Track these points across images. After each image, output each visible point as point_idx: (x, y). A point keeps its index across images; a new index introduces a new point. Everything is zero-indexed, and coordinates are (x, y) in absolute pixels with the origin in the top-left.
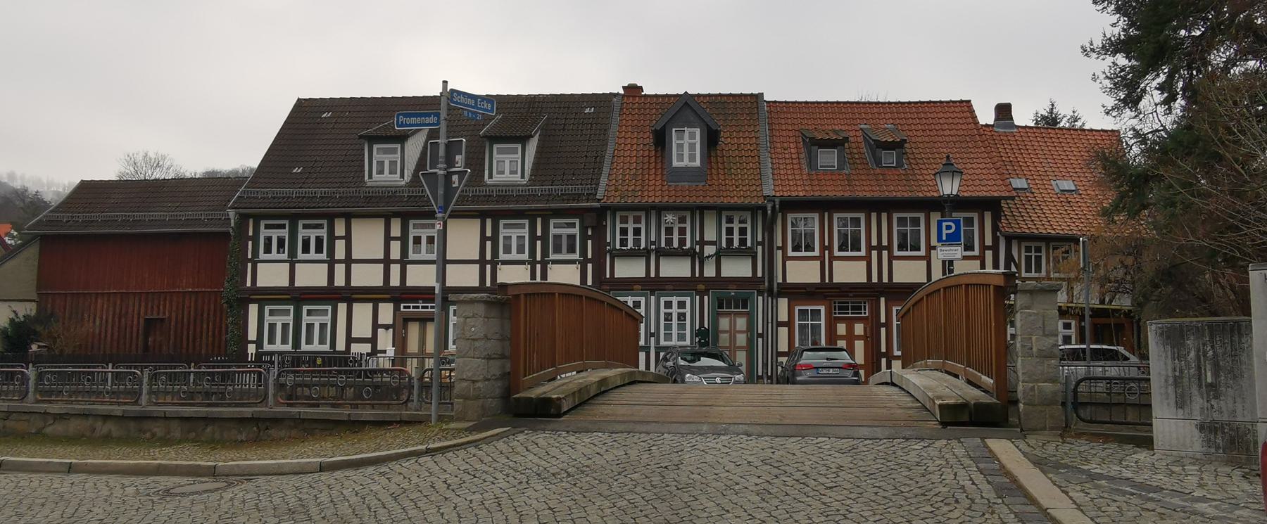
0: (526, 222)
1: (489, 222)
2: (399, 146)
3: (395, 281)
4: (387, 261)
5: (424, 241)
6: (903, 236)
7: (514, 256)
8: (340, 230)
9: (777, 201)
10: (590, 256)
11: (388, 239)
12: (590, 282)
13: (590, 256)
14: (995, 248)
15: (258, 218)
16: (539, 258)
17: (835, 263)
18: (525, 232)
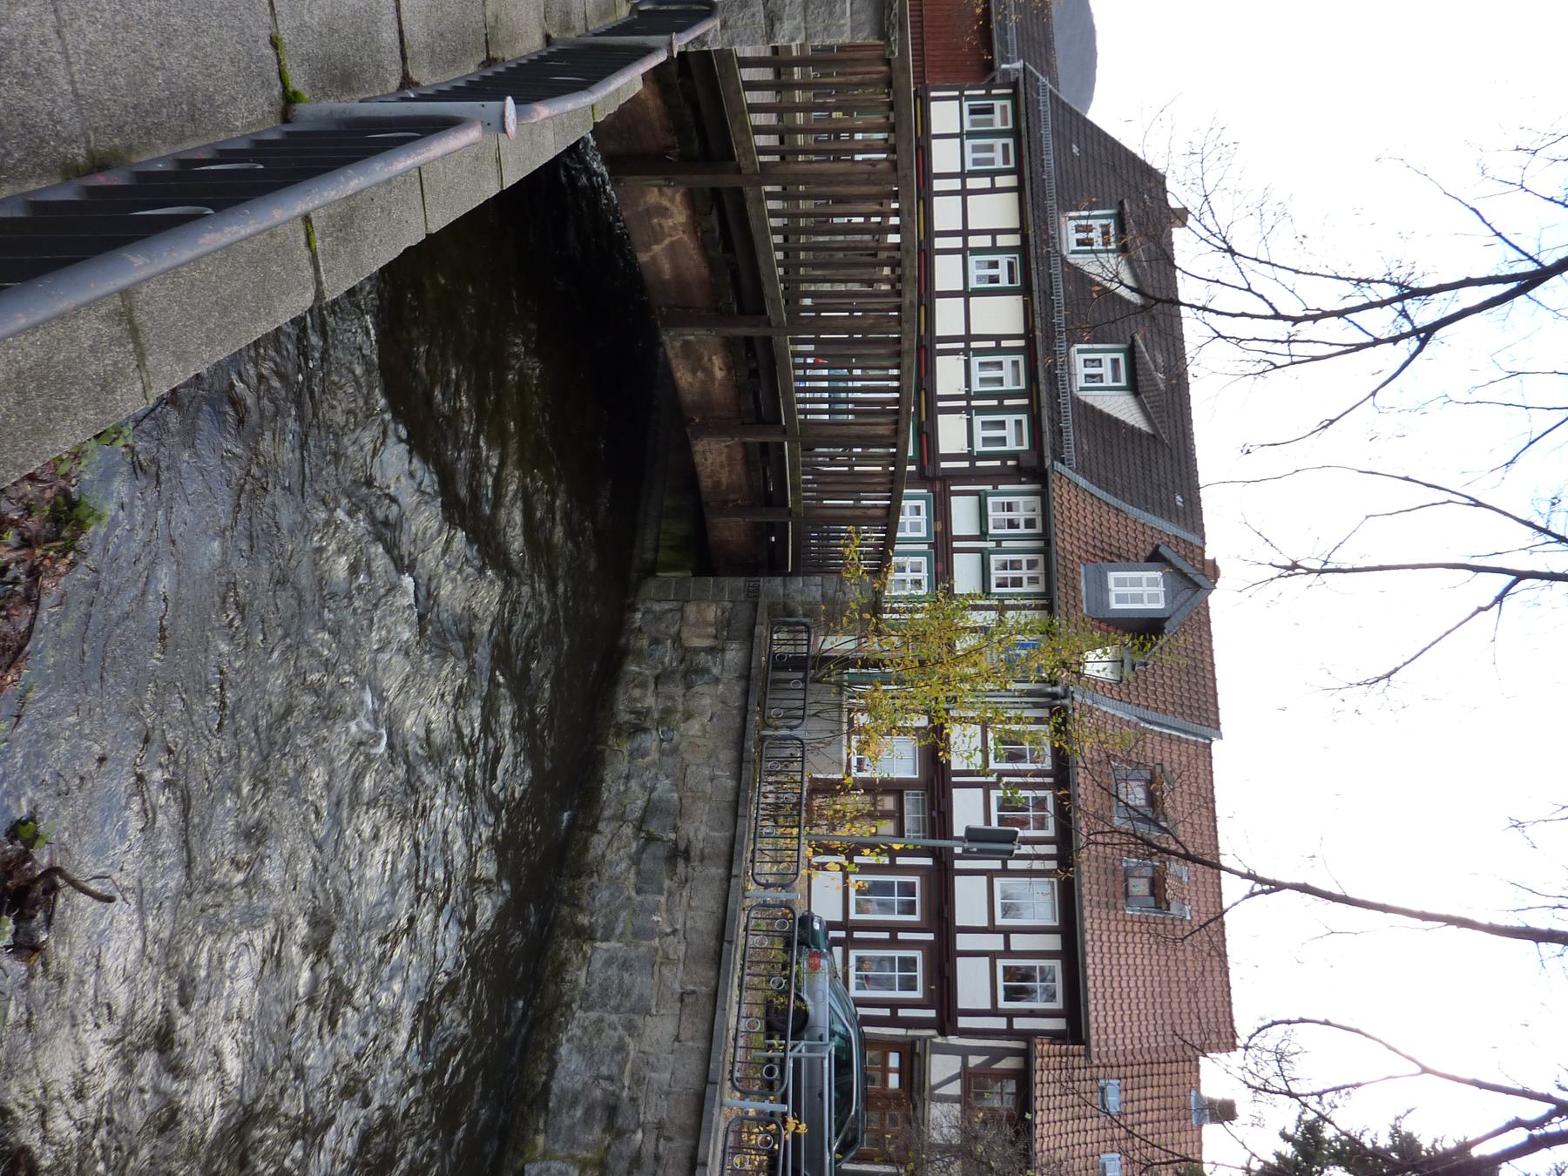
0: (1022, 386)
1: (1021, 343)
2: (1123, 383)
3: (939, 243)
4: (965, 233)
5: (993, 272)
6: (1027, 975)
7: (977, 374)
8: (1001, 181)
9: (1066, 702)
10: (979, 464)
11: (994, 233)
12: (944, 465)
13: (979, 464)
14: (1010, 1033)
15: (1014, 97)
16: (974, 403)
17: (980, 791)
18: (1008, 385)
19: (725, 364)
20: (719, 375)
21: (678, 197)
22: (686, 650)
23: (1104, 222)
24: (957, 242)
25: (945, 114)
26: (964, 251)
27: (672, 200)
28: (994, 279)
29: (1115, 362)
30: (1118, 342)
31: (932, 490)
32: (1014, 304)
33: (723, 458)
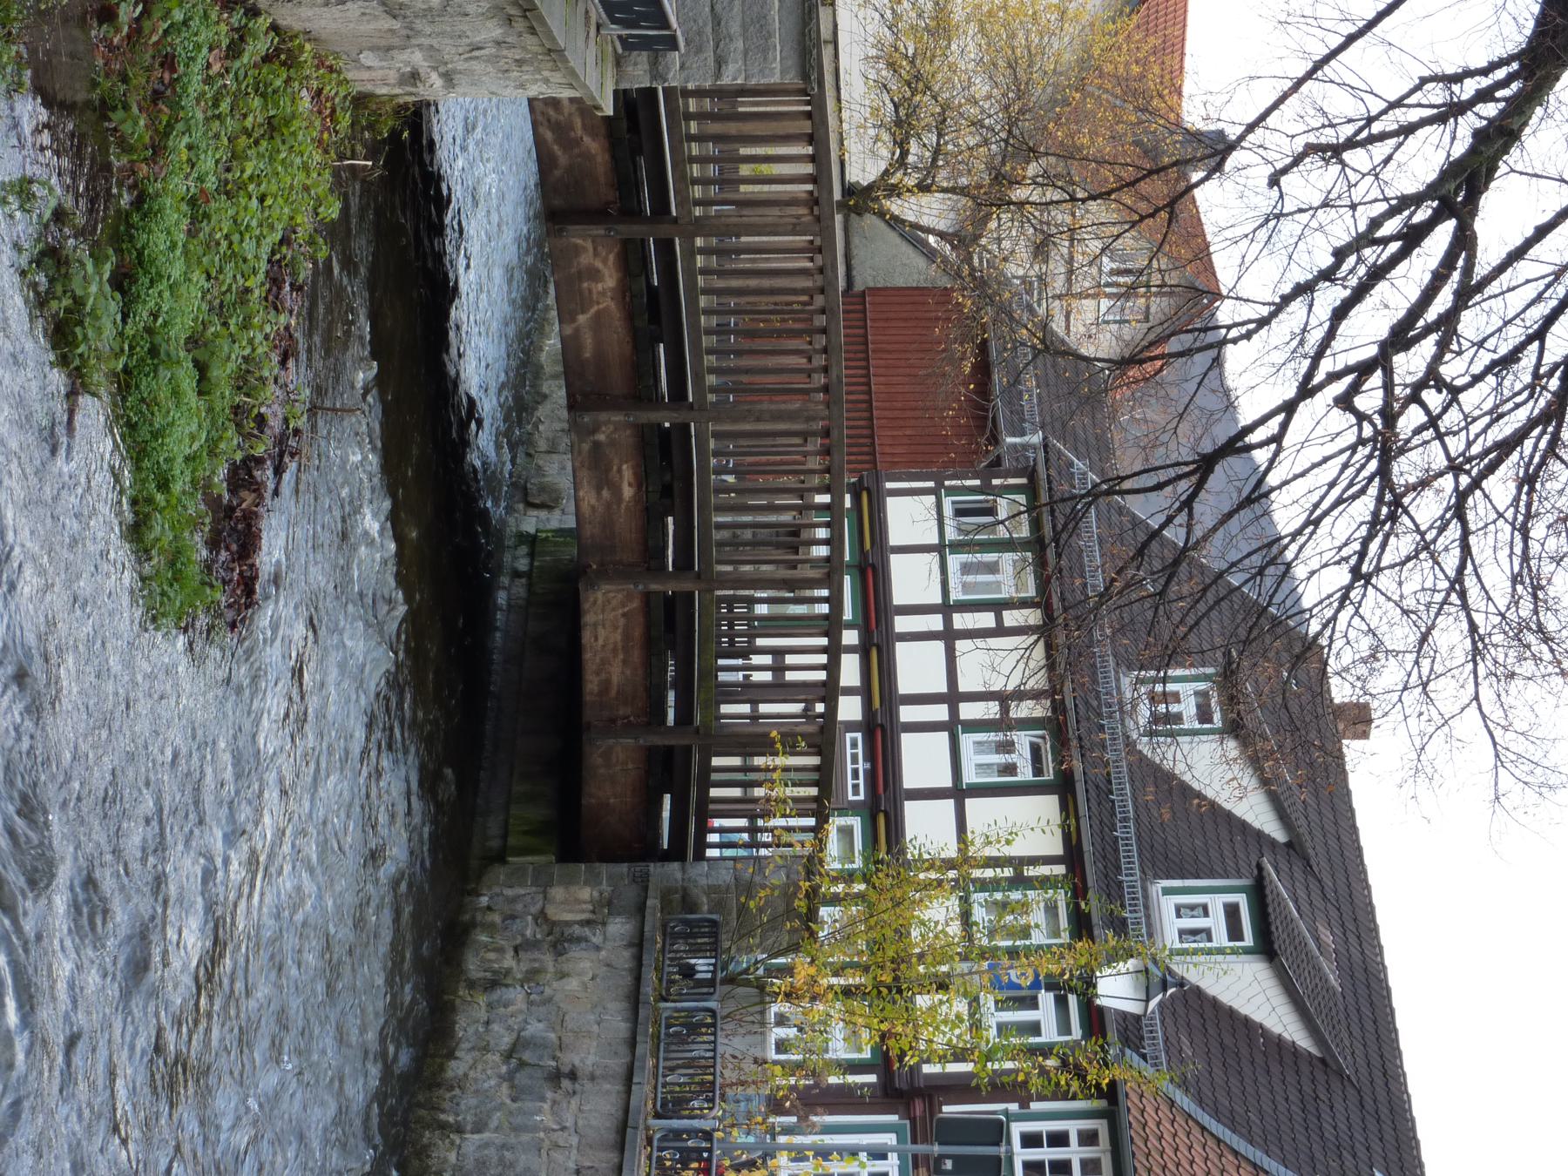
1: (1060, 870)
2: (1249, 940)
3: (907, 714)
4: (953, 697)
8: (1011, 618)
11: (1003, 698)
15: (1031, 490)
19: (635, 474)
20: (628, 492)
21: (611, 257)
22: (554, 923)
23: (1202, 686)
24: (940, 713)
25: (909, 516)
26: (953, 727)
27: (605, 261)
28: (1010, 769)
29: (1232, 912)
30: (1239, 876)
31: (908, 1114)
32: (1048, 806)
33: (618, 636)
